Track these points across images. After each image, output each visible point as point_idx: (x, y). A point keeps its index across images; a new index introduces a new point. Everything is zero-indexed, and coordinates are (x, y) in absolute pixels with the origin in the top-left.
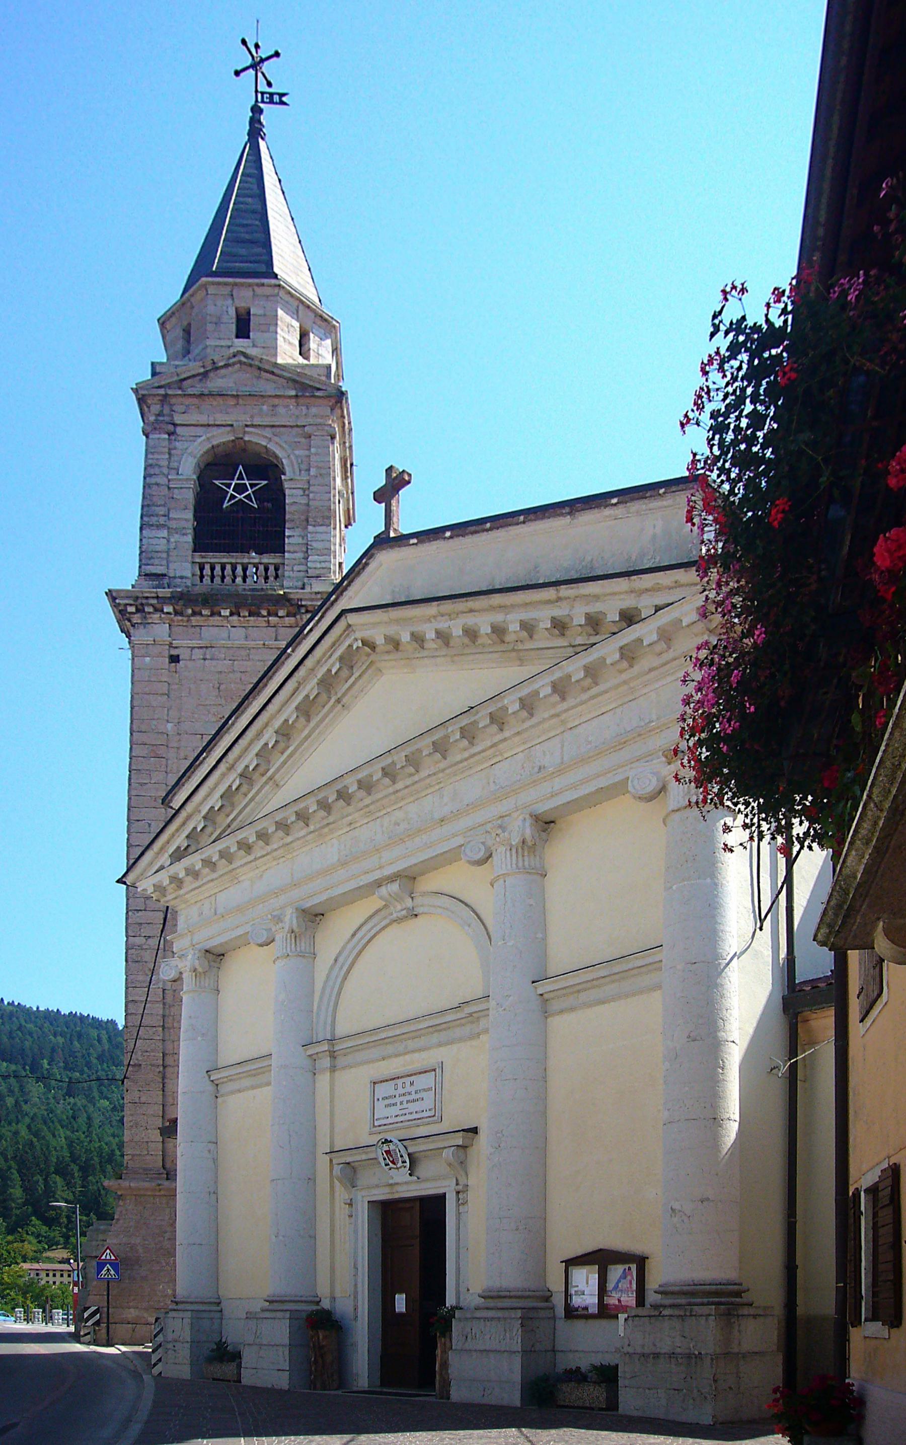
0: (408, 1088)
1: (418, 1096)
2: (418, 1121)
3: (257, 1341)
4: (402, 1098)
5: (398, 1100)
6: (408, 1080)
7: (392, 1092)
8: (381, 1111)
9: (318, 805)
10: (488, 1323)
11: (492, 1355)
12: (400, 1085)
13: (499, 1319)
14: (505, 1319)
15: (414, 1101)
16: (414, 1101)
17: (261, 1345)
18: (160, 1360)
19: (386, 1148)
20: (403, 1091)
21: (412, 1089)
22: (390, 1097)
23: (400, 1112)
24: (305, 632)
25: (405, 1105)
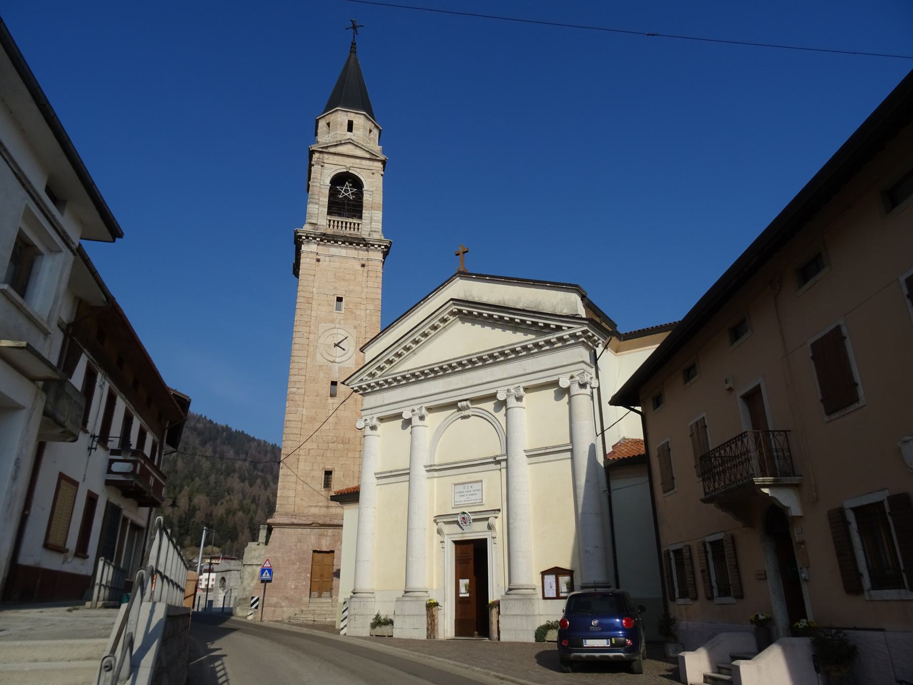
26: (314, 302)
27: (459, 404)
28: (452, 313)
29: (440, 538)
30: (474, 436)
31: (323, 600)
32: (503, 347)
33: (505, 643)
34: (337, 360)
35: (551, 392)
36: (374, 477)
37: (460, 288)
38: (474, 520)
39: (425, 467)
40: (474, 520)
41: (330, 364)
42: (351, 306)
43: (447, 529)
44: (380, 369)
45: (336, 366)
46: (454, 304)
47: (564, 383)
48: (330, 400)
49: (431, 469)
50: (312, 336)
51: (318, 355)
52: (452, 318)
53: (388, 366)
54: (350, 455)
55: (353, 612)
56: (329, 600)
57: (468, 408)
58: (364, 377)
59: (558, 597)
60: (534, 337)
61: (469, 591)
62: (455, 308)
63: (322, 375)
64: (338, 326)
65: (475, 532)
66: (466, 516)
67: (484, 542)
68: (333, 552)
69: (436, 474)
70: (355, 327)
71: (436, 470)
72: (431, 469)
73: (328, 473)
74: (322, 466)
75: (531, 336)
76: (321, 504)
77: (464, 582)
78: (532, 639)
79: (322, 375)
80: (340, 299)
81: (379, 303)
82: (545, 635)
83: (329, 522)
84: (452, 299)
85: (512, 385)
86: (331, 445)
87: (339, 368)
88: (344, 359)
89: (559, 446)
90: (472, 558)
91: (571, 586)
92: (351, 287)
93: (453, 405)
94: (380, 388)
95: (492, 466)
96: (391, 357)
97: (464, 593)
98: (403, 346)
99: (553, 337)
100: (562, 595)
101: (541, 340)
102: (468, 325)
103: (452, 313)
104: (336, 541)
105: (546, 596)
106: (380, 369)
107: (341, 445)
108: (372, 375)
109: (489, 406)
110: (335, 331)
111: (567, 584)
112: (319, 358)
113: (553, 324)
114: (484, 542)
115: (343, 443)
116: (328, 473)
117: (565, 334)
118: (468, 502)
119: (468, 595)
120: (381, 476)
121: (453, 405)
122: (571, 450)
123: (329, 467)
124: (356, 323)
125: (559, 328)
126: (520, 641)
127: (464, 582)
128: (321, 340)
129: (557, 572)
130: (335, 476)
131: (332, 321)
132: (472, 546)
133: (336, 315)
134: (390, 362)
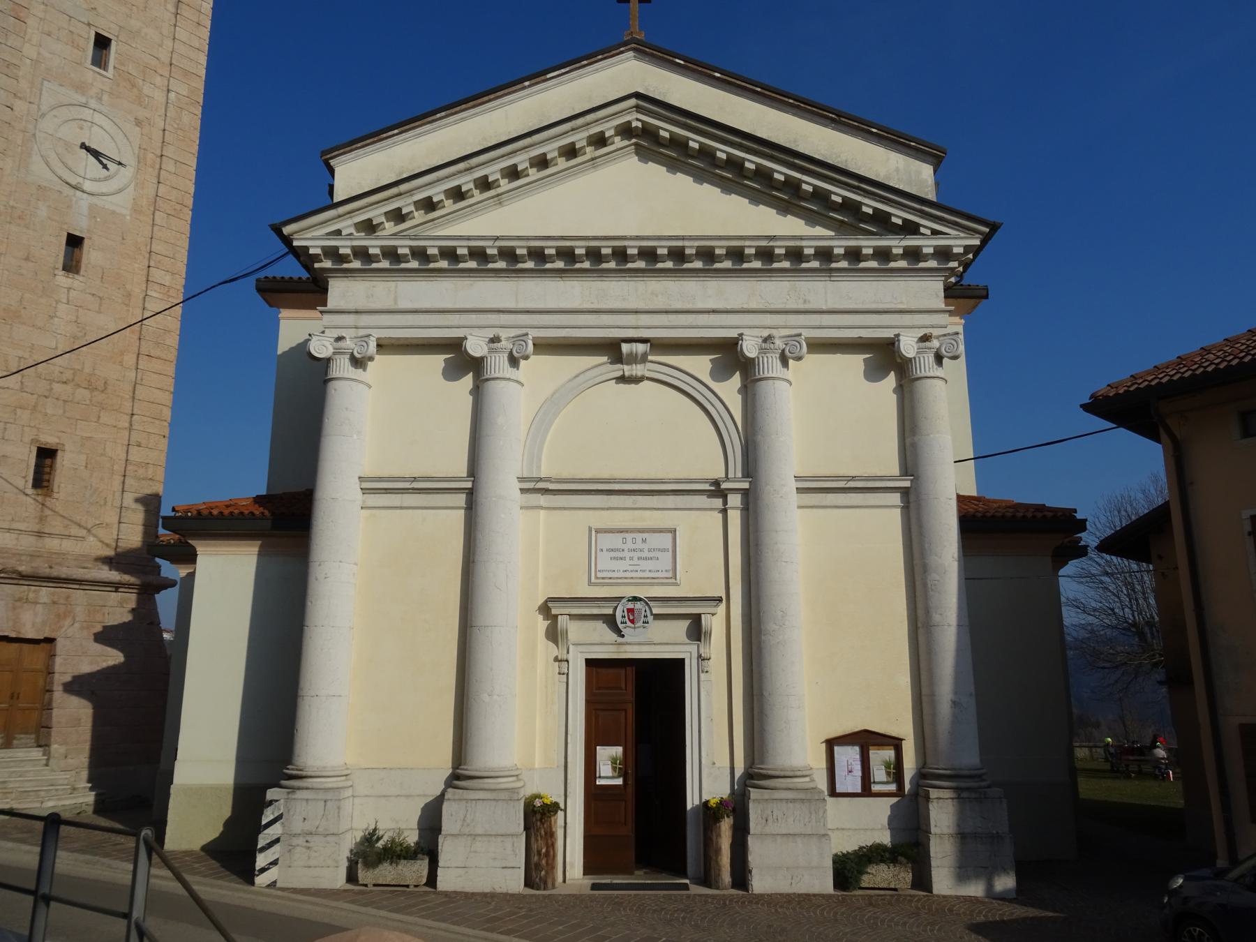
0: (639, 545)
1: (651, 555)
2: (653, 582)
3: (466, 830)
4: (632, 554)
5: (627, 554)
6: (639, 536)
7: (620, 546)
8: (605, 563)
9: (324, 290)
10: (791, 805)
11: (799, 840)
12: (639, 540)
13: (802, 800)
14: (809, 800)
15: (646, 559)
16: (646, 559)
17: (474, 836)
18: (275, 863)
19: (630, 606)
20: (633, 546)
21: (645, 546)
22: (618, 550)
23: (630, 568)
24: (549, 76)
25: (636, 561)
26: (31, 22)
27: (625, 348)
28: (626, 131)
29: (553, 650)
30: (660, 426)
31: (20, 754)
32: (683, 238)
33: (774, 901)
34: (87, 186)
35: (438, 361)
36: (356, 486)
37: (626, 74)
38: (658, 617)
39: (521, 479)
40: (658, 617)
41: (71, 191)
42: (131, 68)
43: (576, 631)
44: (398, 216)
45: (84, 202)
46: (638, 108)
47: (476, 347)
48: (63, 279)
49: (535, 487)
50: (20, 106)
51: (36, 158)
52: (619, 142)
53: (419, 216)
54: (106, 418)
55: (297, 826)
56: (36, 754)
57: (643, 359)
58: (347, 226)
59: (867, 790)
60: (832, 233)
61: (623, 773)
62: (636, 120)
63: (43, 211)
64: (93, 103)
65: (656, 641)
66: (638, 605)
67: (675, 668)
68: (50, 641)
69: (543, 500)
70: (138, 123)
71: (546, 491)
72: (535, 487)
73: (46, 455)
74: (29, 435)
75: (819, 231)
76: (22, 526)
77: (607, 755)
78: (825, 884)
79: (43, 211)
80: (102, 43)
81: (200, 85)
82: (861, 873)
83: (46, 571)
84: (637, 95)
85: (782, 328)
86: (57, 387)
87: (92, 207)
88: (103, 187)
89: (881, 478)
90: (639, 704)
91: (896, 771)
92: (135, 24)
93: (611, 349)
94: (424, 262)
95: (702, 501)
96: (437, 193)
97: (607, 775)
98: (479, 174)
99: (897, 244)
100: (875, 788)
101: (839, 246)
102: (656, 171)
103: (626, 131)
104: (60, 617)
105: (839, 789)
106: (398, 216)
107: (86, 393)
108: (369, 227)
109: (700, 365)
110: (86, 114)
111: (887, 765)
112: (38, 167)
113: (898, 216)
114: (675, 668)
115: (91, 388)
116: (46, 455)
117: (928, 245)
118: (627, 572)
119: (619, 782)
120: (375, 487)
121: (611, 349)
122: (905, 492)
123: (49, 440)
124: (142, 114)
125: (910, 229)
126: (803, 891)
127: (607, 755)
128: (47, 125)
129: (866, 740)
130: (64, 462)
131: (81, 88)
132: (631, 671)
133: (90, 73)
134: (429, 205)
